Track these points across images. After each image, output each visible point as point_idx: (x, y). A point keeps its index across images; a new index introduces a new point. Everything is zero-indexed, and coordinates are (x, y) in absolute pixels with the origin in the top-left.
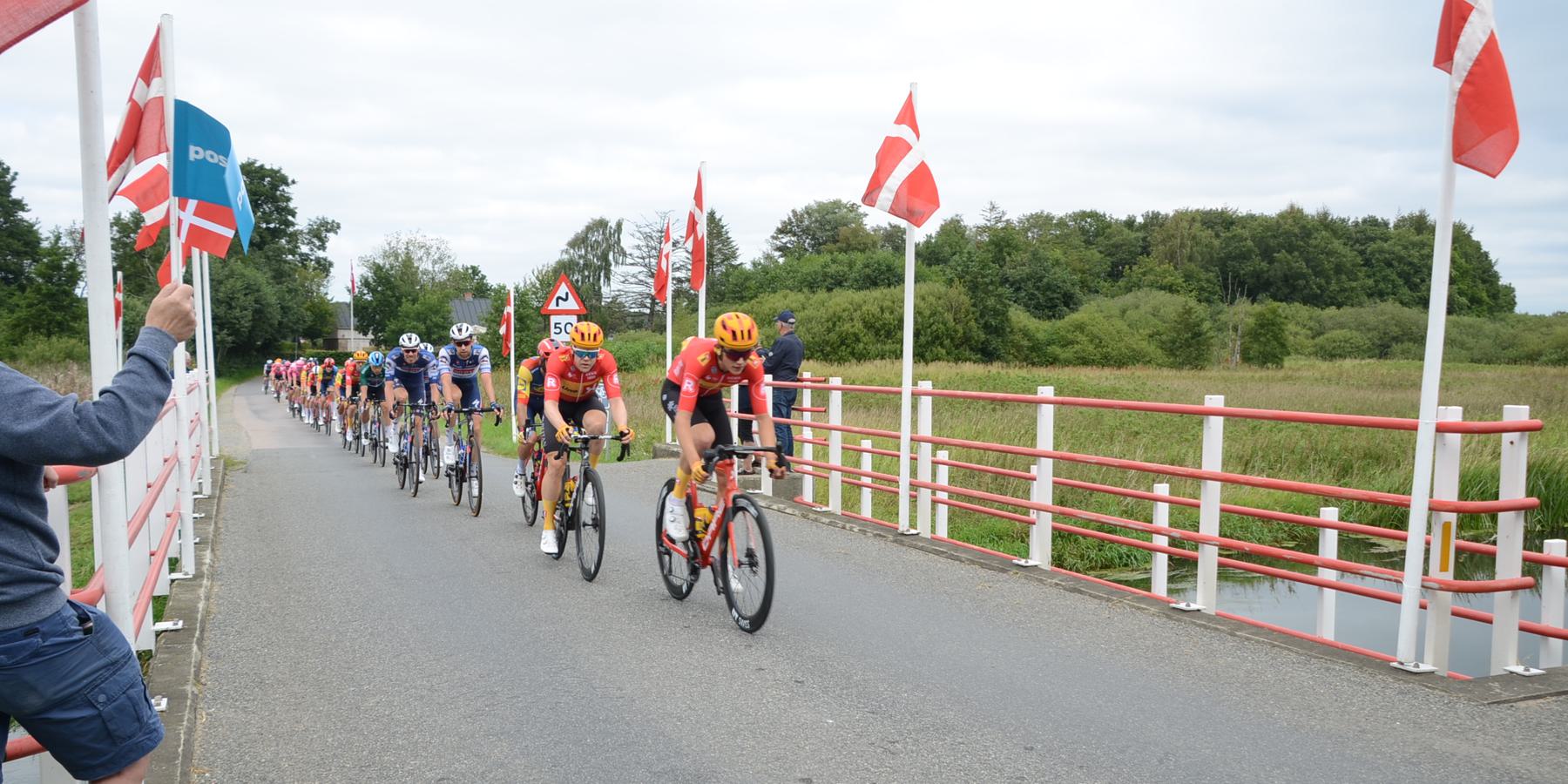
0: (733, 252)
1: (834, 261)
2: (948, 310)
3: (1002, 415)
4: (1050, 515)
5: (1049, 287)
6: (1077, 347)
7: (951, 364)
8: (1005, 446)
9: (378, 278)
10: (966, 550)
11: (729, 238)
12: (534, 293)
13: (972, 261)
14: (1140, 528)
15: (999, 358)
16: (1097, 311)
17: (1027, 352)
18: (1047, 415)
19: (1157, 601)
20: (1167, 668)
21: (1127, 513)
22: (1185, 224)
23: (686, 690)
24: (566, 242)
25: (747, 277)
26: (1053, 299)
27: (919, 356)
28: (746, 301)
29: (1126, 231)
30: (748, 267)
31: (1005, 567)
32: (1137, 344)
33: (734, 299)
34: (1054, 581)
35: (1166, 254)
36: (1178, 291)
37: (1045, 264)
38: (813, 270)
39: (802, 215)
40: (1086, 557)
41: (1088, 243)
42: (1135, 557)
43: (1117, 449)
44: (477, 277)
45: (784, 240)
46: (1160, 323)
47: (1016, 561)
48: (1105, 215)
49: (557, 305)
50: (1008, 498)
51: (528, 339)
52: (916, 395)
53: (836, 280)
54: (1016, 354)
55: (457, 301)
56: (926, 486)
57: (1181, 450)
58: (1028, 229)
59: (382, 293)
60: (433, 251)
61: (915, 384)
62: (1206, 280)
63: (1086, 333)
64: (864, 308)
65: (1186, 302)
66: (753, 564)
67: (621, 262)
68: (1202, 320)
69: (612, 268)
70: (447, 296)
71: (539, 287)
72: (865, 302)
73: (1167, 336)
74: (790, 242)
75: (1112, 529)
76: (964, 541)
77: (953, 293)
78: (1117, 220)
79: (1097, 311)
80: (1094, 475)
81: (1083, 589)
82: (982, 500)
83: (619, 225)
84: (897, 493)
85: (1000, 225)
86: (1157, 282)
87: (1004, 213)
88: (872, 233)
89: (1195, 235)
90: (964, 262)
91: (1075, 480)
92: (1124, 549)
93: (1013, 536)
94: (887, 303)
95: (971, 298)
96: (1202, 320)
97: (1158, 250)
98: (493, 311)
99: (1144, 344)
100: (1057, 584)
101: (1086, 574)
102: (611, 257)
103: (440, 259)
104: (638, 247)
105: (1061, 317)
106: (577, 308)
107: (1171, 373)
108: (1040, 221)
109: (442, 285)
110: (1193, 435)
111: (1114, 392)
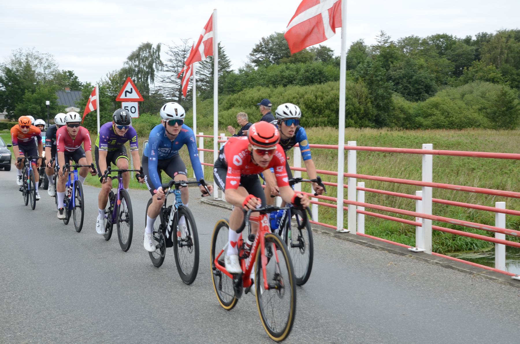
0: (227, 63)
1: (287, 69)
2: (355, 97)
3: (390, 160)
4: (430, 221)
5: (416, 82)
6: (434, 118)
7: (357, 129)
8: (391, 179)
9: (9, 77)
10: (379, 242)
11: (225, 55)
12: (108, 88)
13: (370, 67)
14: (478, 227)
15: (386, 125)
16: (446, 96)
17: (403, 121)
18: (428, 162)
19: (500, 274)
20: (515, 317)
21: (470, 218)
22: (504, 40)
23: (219, 329)
24: (127, 57)
25: (236, 78)
26: (419, 89)
27: (347, 126)
28: (236, 93)
29: (465, 46)
30: (237, 72)
31: (403, 253)
32: (471, 115)
33: (228, 91)
34: (435, 261)
35: (491, 59)
36: (498, 82)
37: (414, 68)
38: (275, 74)
39: (268, 41)
40: (445, 245)
41: (441, 54)
42: (476, 245)
43: (462, 179)
44: (72, 78)
45: (258, 56)
46: (486, 102)
47: (410, 249)
48: (452, 36)
49: (126, 96)
50: (396, 209)
51: (106, 115)
52: (347, 150)
53: (289, 79)
54: (396, 122)
55: (60, 92)
56: (353, 204)
57: (503, 179)
58: (404, 47)
59: (12, 86)
60: (44, 61)
61: (346, 142)
62: (517, 74)
63: (439, 109)
64: (306, 97)
65: (503, 88)
66: (279, 287)
67: (160, 69)
68: (513, 99)
69: (155, 73)
70: (54, 89)
71: (111, 84)
72: (306, 93)
73: (491, 109)
74: (261, 57)
75: (461, 227)
76: (370, 235)
77: (358, 86)
78: (459, 39)
79: (446, 96)
80: (449, 195)
81: (453, 266)
82: (393, 213)
83: (159, 47)
84: (336, 208)
85: (387, 45)
86: (484, 77)
87: (389, 38)
88: (310, 51)
89: (511, 46)
90: (365, 68)
91: (437, 198)
92: (469, 240)
93: (400, 232)
94: (320, 93)
95: (369, 89)
96: (513, 99)
97: (486, 57)
98: (84, 99)
99: (476, 115)
100: (437, 263)
101: (445, 254)
102: (154, 66)
103: (48, 66)
104: (171, 60)
105: (424, 100)
106: (138, 97)
107: (493, 133)
108: (412, 42)
109: (51, 82)
110: (510, 170)
111: (458, 145)
